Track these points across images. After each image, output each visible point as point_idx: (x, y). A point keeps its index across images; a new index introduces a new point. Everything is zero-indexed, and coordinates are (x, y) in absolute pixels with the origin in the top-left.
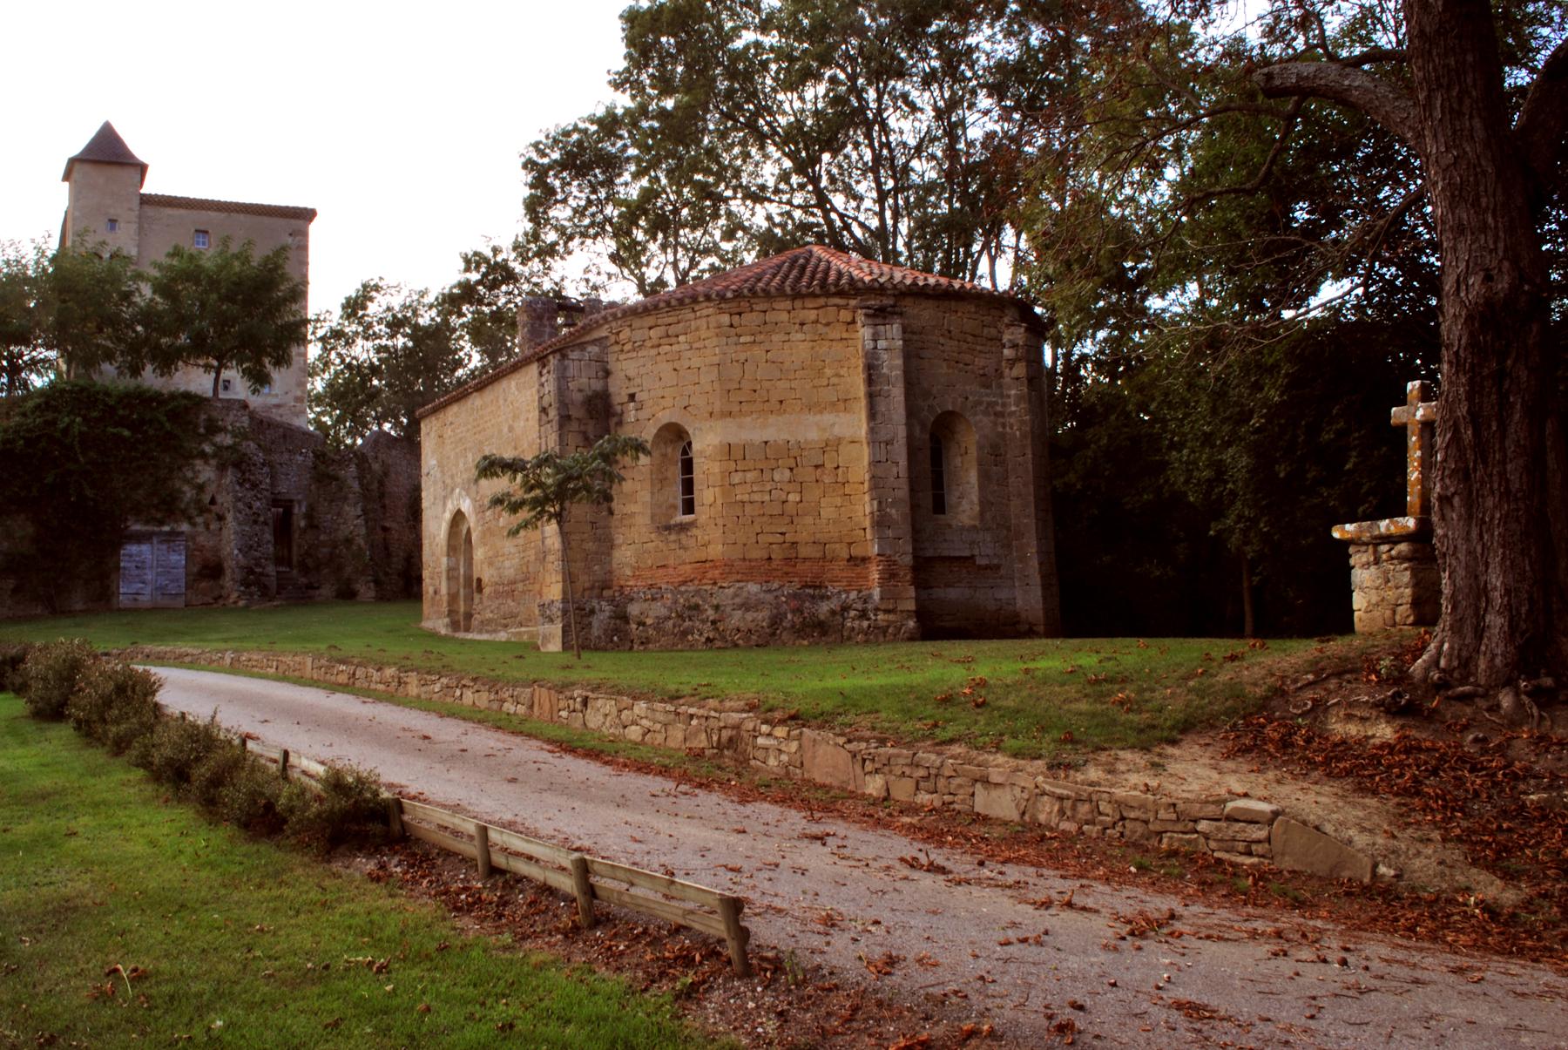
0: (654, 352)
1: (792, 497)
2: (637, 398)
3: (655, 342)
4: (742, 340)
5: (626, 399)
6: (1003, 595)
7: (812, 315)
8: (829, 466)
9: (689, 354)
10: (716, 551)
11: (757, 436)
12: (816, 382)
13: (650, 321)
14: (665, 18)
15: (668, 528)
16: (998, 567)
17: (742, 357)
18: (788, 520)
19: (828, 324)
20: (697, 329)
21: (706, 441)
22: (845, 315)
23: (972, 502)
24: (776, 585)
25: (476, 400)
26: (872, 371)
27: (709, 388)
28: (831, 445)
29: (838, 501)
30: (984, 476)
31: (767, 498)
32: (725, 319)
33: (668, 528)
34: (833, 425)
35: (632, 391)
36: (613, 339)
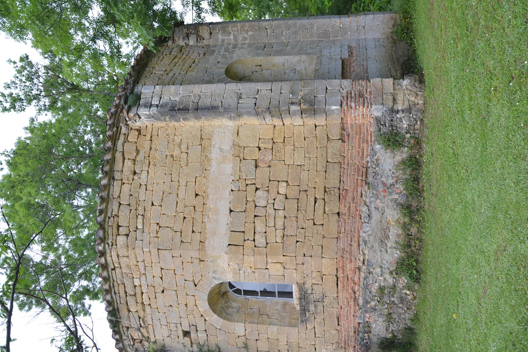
0: (148, 308)
1: (282, 191)
2: (187, 329)
3: (140, 307)
4: (140, 226)
5: (187, 339)
6: (372, 53)
7: (128, 163)
8: (256, 155)
9: (150, 277)
10: (328, 266)
11: (224, 218)
12: (183, 163)
13: (123, 312)
14: (114, 319)
15: (304, 310)
16: (350, 47)
17: (155, 227)
18: (303, 195)
19: (138, 152)
20: (129, 267)
21: (225, 268)
22: (133, 136)
23: (299, 62)
24: (365, 209)
25: (431, 237)
26: (176, 110)
27: (178, 261)
28: (239, 153)
29: (289, 148)
30: (280, 53)
31: (281, 213)
32: (121, 240)
33: (304, 310)
34: (221, 150)
35: (181, 334)
36: (137, 345)
